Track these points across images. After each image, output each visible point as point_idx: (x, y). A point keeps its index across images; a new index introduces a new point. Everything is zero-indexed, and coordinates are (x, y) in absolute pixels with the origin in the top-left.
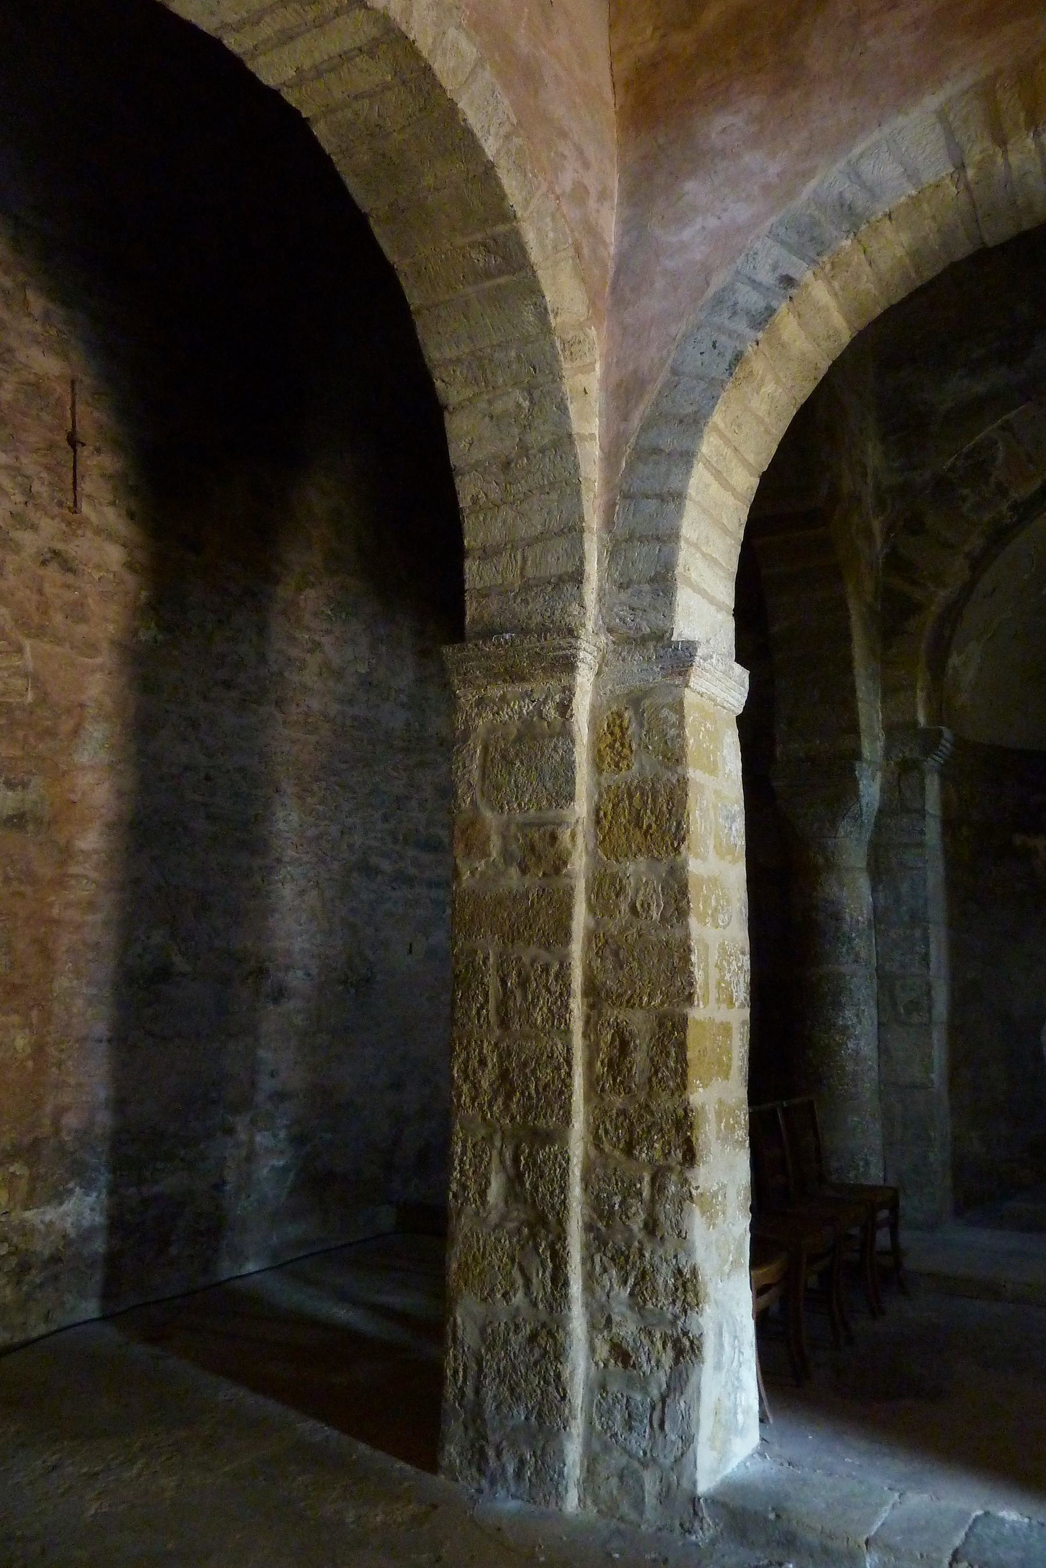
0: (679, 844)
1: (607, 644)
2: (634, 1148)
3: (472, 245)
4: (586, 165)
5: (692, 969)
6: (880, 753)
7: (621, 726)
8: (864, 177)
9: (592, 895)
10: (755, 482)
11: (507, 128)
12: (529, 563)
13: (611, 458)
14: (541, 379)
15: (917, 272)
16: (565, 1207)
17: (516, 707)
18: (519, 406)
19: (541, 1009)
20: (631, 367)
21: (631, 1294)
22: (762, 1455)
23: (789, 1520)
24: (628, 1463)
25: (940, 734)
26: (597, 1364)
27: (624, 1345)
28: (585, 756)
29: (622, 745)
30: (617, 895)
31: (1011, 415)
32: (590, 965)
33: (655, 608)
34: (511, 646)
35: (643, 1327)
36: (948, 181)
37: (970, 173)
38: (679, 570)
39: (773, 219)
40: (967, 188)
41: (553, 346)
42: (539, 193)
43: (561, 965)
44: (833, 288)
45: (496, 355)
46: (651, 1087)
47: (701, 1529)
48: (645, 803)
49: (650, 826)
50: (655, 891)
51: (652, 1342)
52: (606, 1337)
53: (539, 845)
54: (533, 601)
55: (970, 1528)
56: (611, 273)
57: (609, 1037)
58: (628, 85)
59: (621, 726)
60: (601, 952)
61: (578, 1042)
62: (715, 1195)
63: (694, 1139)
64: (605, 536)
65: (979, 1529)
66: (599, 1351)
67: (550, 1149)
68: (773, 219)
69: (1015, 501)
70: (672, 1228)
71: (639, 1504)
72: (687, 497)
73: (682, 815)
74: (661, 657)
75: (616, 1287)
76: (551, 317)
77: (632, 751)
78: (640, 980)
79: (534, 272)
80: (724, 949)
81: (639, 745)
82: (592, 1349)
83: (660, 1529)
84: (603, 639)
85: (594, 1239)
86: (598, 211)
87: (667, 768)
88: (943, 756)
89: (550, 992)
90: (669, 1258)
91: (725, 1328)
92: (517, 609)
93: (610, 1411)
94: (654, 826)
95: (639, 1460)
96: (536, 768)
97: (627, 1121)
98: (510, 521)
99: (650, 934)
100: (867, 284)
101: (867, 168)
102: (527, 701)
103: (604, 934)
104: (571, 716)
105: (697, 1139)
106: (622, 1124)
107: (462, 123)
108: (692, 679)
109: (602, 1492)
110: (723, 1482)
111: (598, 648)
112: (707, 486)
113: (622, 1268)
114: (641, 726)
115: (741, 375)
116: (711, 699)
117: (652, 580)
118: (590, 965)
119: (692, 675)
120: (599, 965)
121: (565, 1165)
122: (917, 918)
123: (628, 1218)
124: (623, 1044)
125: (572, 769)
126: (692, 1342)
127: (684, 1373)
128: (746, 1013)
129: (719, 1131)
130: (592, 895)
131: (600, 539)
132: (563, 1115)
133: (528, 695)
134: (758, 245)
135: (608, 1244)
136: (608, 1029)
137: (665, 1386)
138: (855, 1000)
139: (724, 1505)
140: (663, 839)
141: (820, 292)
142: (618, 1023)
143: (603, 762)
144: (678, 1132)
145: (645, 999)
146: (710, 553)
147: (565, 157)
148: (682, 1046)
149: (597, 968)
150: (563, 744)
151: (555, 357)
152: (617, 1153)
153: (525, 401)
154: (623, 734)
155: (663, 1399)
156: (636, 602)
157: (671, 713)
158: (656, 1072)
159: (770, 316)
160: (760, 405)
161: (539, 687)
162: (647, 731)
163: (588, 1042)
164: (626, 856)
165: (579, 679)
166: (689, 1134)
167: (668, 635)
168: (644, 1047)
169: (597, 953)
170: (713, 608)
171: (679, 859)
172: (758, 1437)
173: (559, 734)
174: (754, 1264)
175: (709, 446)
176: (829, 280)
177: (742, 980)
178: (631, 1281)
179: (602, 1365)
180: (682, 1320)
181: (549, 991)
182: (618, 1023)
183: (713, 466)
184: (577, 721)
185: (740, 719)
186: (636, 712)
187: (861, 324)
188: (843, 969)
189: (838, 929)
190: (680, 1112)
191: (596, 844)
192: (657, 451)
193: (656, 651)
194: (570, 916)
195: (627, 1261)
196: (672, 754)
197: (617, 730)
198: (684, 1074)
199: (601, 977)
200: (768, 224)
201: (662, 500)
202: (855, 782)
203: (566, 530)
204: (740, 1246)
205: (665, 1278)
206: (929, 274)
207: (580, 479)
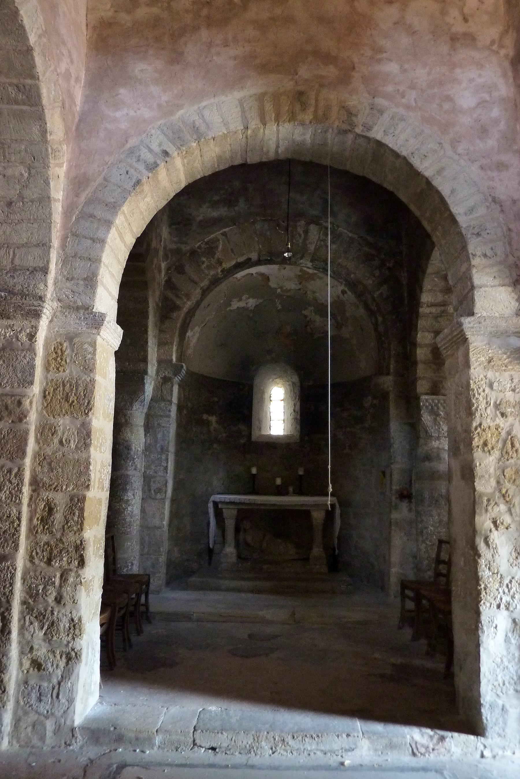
0: (88, 411)
1: (57, 307)
2: (52, 561)
3: (10, 84)
4: (72, 62)
5: (90, 473)
6: (154, 372)
7: (61, 350)
8: (205, 117)
9: (39, 434)
10: (134, 241)
11: (40, 32)
12: (17, 257)
13: (67, 212)
14: (36, 164)
15: (218, 165)
16: (12, 594)
17: (3, 332)
18: (22, 175)
19: (5, 492)
20: (82, 171)
21: (45, 634)
22: (101, 703)
23: (121, 729)
24: (38, 718)
25: (182, 367)
26: (23, 672)
27: (39, 660)
28: (40, 362)
29: (61, 359)
30: (52, 435)
31: (226, 230)
32: (34, 469)
33: (85, 294)
34: (4, 300)
35: (50, 649)
36: (240, 132)
37: (249, 132)
38: (99, 277)
39: (162, 122)
40: (247, 137)
41: (47, 150)
42: (50, 69)
43: (19, 469)
44: (184, 162)
45: (13, 145)
46: (64, 531)
47: (76, 742)
48: (72, 390)
49: (73, 402)
50: (73, 434)
51: (55, 656)
52: (29, 657)
53: (11, 407)
54: (18, 277)
55: (198, 717)
56: (77, 120)
57: (43, 506)
58: (95, 28)
59: (61, 350)
60: (41, 463)
61: (25, 509)
62: (91, 581)
63: (84, 555)
64: (61, 252)
65: (202, 716)
66: (24, 665)
67: (5, 564)
68: (162, 122)
69: (224, 269)
70: (70, 599)
71: (43, 738)
72: (107, 242)
73: (91, 397)
74: (87, 318)
75: (37, 631)
76: (48, 135)
77: (66, 363)
78: (62, 478)
79: (43, 110)
80: (103, 463)
81: (71, 360)
82: (21, 664)
83: (53, 747)
84: (55, 304)
85: (26, 608)
86: (74, 86)
87: (85, 373)
88: (182, 377)
89: (11, 484)
90: (67, 614)
91: (90, 644)
92: (8, 280)
93: (29, 694)
94: (76, 401)
95: (44, 716)
96: (12, 366)
97: (49, 548)
98: (8, 233)
99: (70, 455)
100: (198, 165)
101: (206, 113)
102: (10, 330)
103: (43, 454)
104: (36, 341)
105: (86, 555)
106: (46, 550)
107: (20, 21)
108: (102, 331)
109: (23, 735)
110: (85, 719)
111: (52, 308)
112: (115, 239)
113: (41, 621)
114: (73, 351)
115: (138, 191)
116: (107, 342)
117: (85, 279)
118: (34, 469)
119: (102, 329)
120: (40, 470)
121: (13, 572)
122: (164, 450)
123: (46, 596)
124: (50, 509)
125: (33, 369)
126: (76, 654)
127: (71, 669)
128: (108, 494)
129: (94, 551)
130: (39, 434)
131: (58, 253)
132: (14, 546)
133: (11, 327)
134: (153, 131)
135: (34, 610)
136: (42, 502)
137: (60, 677)
138: (133, 487)
139: (88, 729)
140: (80, 408)
141: (178, 162)
142: (48, 500)
143: (50, 366)
144: (76, 552)
145: (64, 487)
146: (112, 271)
147: (63, 55)
148: (82, 510)
149: (39, 471)
150: (29, 355)
151: (47, 156)
152: (42, 564)
153: (26, 172)
154: (62, 354)
155: (59, 683)
156: (75, 288)
157: (89, 347)
158: (67, 523)
159: (156, 167)
160: (143, 206)
161: (18, 323)
162: (76, 354)
163: (30, 509)
164: (59, 415)
165: (41, 323)
166: (82, 552)
167: (91, 308)
168: (62, 511)
169: (39, 464)
170: (110, 298)
171: (88, 419)
172: (98, 695)
173: (29, 350)
174: (102, 612)
175: (119, 220)
176: (183, 158)
177: (108, 478)
178: (46, 627)
179: (26, 672)
180: (72, 643)
181: (10, 482)
182: (48, 500)
183: (119, 230)
184: (38, 344)
185: (116, 353)
186: (70, 344)
187: (191, 181)
188: (129, 473)
189: (129, 453)
190: (79, 542)
191: (42, 408)
192: (92, 216)
193: (84, 314)
194: (26, 444)
195: (44, 618)
196: (88, 367)
197: (59, 352)
198: (82, 524)
199: (40, 476)
200: (159, 123)
201: (94, 241)
202: (143, 384)
203: (41, 245)
204: (97, 605)
205: (64, 623)
206: (222, 168)
207: (52, 221)
